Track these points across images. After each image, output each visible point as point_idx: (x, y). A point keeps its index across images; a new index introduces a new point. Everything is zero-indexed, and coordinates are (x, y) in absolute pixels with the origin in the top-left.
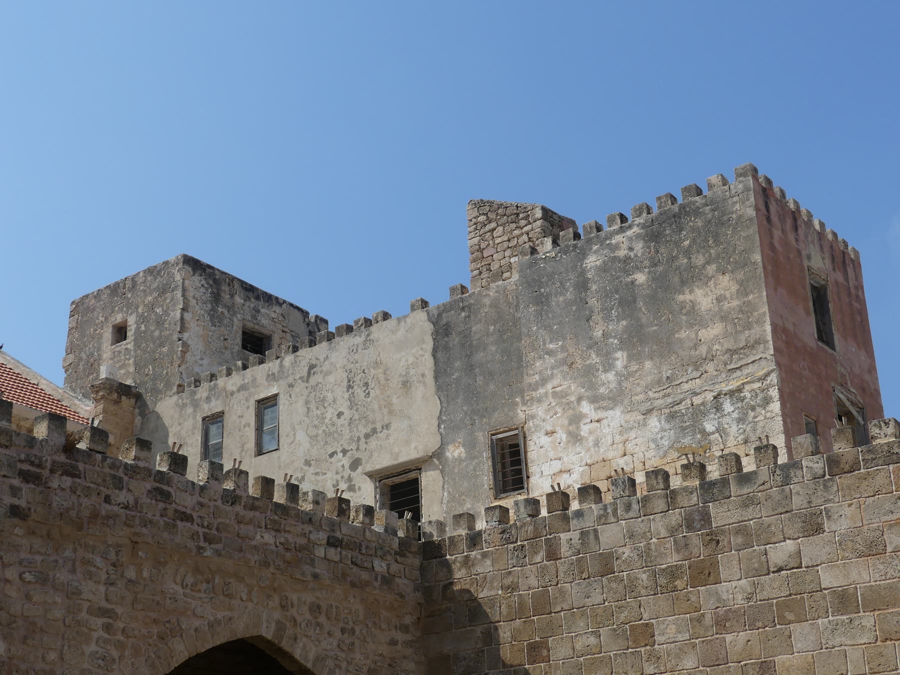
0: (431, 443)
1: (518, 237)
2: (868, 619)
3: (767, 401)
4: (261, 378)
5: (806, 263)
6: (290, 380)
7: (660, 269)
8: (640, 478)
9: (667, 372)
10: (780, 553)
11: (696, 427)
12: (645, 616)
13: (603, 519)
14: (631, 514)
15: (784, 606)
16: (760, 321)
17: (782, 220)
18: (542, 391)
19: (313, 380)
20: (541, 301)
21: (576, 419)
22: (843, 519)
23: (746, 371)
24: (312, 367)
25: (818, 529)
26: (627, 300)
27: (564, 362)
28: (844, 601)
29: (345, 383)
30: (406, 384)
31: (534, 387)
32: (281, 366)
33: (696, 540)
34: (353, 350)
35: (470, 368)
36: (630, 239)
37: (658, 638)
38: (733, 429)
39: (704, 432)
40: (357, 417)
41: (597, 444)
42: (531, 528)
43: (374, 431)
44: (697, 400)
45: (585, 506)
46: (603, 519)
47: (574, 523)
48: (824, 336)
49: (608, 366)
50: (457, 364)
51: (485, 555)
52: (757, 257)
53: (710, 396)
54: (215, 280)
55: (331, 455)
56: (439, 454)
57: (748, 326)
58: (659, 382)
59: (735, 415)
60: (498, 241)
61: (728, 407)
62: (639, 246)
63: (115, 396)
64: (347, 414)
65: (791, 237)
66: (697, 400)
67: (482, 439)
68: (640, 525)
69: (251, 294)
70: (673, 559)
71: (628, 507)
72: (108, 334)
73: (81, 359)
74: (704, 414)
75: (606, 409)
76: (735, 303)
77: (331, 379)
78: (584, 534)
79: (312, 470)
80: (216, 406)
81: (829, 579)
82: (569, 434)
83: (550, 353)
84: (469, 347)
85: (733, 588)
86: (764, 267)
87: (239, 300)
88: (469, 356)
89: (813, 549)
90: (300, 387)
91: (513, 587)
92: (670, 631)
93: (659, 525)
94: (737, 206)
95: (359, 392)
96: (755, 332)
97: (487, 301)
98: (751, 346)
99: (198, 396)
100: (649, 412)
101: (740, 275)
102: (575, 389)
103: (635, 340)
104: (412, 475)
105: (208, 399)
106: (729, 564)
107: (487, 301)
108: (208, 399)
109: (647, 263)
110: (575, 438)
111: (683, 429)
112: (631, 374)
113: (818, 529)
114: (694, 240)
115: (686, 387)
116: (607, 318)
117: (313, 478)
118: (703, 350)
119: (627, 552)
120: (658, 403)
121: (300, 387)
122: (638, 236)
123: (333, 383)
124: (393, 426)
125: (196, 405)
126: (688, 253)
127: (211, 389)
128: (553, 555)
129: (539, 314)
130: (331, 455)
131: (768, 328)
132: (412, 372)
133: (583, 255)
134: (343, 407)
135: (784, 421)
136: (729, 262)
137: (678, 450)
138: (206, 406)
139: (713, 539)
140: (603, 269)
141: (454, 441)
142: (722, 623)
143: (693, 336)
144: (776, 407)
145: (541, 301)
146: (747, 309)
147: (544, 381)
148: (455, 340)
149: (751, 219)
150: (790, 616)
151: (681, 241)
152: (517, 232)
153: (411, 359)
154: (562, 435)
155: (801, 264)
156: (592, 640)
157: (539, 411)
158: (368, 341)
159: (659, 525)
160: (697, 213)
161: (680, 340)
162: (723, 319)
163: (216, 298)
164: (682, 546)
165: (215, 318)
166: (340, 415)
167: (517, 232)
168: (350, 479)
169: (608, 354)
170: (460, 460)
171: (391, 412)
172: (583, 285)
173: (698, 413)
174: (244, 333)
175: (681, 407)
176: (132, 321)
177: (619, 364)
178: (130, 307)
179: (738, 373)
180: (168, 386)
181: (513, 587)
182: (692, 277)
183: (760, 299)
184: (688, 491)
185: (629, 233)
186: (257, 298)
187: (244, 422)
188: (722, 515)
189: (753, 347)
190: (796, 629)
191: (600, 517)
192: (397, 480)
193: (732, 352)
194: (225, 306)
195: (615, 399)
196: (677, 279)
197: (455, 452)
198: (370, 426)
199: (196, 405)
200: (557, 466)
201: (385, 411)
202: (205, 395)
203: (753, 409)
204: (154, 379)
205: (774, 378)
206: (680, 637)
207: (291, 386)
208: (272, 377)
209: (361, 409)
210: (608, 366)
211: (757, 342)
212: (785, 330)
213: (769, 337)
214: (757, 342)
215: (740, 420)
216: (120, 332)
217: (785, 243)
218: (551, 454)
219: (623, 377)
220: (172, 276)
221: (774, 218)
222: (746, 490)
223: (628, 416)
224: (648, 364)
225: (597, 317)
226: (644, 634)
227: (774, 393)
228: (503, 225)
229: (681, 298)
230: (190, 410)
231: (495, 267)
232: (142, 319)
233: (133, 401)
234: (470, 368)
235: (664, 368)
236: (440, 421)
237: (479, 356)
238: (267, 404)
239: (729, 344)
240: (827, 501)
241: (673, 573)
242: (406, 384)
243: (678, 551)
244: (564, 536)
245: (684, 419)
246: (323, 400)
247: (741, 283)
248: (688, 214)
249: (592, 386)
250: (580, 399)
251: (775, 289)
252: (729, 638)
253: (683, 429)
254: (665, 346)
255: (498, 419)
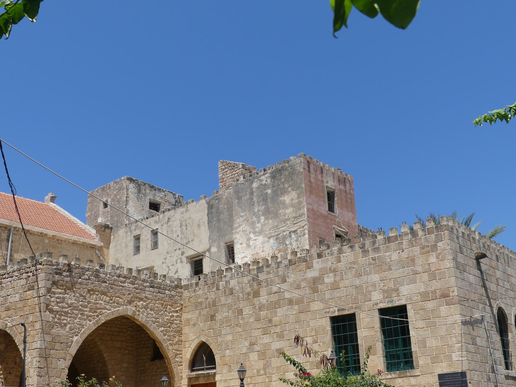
0: (207, 247)
1: (234, 174)
2: (296, 307)
3: (304, 234)
4: (153, 223)
5: (325, 185)
6: (162, 223)
7: (275, 188)
8: (269, 259)
9: (276, 224)
10: (275, 289)
11: (284, 243)
12: (241, 307)
13: (231, 278)
14: (239, 276)
15: (276, 303)
16: (303, 208)
17: (316, 171)
18: (239, 229)
19: (170, 223)
20: (239, 198)
21: (249, 239)
22: (292, 278)
23: (299, 224)
24: (169, 219)
25: (285, 281)
26: (264, 199)
27: (245, 220)
28: (290, 302)
29: (180, 225)
30: (199, 225)
31: (237, 228)
32: (159, 218)
33: (255, 284)
34: (182, 213)
35: (219, 220)
36: (266, 178)
37: (244, 313)
38: (294, 244)
39: (286, 245)
40: (183, 237)
41: (255, 248)
42: (212, 280)
43: (189, 242)
44: (285, 233)
45: (227, 274)
46: (231, 278)
47: (223, 279)
48: (331, 208)
49: (259, 222)
50: (215, 219)
51: (200, 289)
52: (303, 186)
53: (288, 232)
54: (138, 185)
55: (175, 250)
56: (209, 250)
57: (300, 209)
58: (273, 227)
59: (295, 239)
60: (228, 175)
61: (293, 236)
62: (269, 180)
63: (103, 229)
64: (180, 236)
65: (319, 177)
66: (285, 233)
67: (223, 245)
68: (240, 280)
69: (152, 189)
70: (249, 290)
71: (238, 274)
72: (102, 205)
73: (92, 214)
74: (286, 238)
75: (258, 236)
76: (297, 201)
77: (175, 223)
78: (226, 282)
79: (169, 255)
80: (138, 232)
81: (287, 295)
82: (247, 244)
83: (242, 216)
84: (219, 213)
85: (264, 298)
86: (306, 189)
87: (148, 191)
88: (219, 216)
89: (284, 286)
90: (165, 226)
91: (207, 298)
92: (247, 311)
93: (246, 280)
94: (298, 168)
95: (184, 228)
96: (301, 211)
97: (224, 197)
98: (300, 216)
99: (132, 229)
100: (271, 237)
101: (298, 192)
102: (248, 229)
103: (267, 213)
104: (201, 257)
105: (135, 230)
106: (263, 292)
107: (224, 197)
108: (135, 230)
109: (271, 186)
110: (248, 246)
111: (280, 243)
112: (265, 224)
113: (285, 281)
114: (285, 179)
115: (281, 229)
116: (259, 205)
117: (169, 258)
118: (287, 216)
119: (237, 288)
120: (273, 234)
121: (165, 226)
122: (269, 177)
123: (175, 224)
124: (195, 241)
125: (131, 231)
126: (283, 183)
127: (136, 226)
128: (218, 289)
129: (239, 203)
130: (175, 250)
131: (306, 210)
132: (201, 221)
133: (252, 183)
134: (179, 233)
135: (309, 241)
136: (296, 187)
137: (278, 250)
138: (134, 232)
139: (259, 284)
140: (258, 188)
141: (213, 246)
142: (260, 309)
143: (284, 212)
144: (307, 236)
145: (239, 198)
146: (300, 203)
147: (239, 226)
148: (214, 210)
149: (302, 173)
150: (277, 306)
151: (282, 179)
152: (234, 172)
153: (200, 217)
154: (244, 245)
155: (323, 186)
156: (227, 314)
157: (237, 236)
158: (187, 211)
159: (246, 280)
160: (286, 169)
161: (280, 213)
162: (293, 206)
163: (139, 191)
164: (251, 286)
165: (139, 199)
166: (178, 236)
167: (234, 172)
168: (181, 259)
169: (259, 217)
170: (215, 252)
171: (194, 235)
172: (252, 193)
173: (284, 238)
174: (150, 203)
175: (280, 236)
176: (109, 200)
177: (262, 221)
178: (108, 195)
179: (296, 225)
180: (122, 224)
181: (207, 298)
182: (284, 192)
183: (303, 199)
184: (254, 269)
185: (266, 176)
186: (155, 190)
187: (147, 238)
188: (262, 277)
189: (301, 216)
190: (279, 310)
191: (230, 277)
192: (197, 259)
193: (295, 218)
194: (143, 194)
195: (261, 233)
196: (280, 192)
197: (214, 249)
198: (188, 240)
199: (131, 231)
200: (243, 255)
201: (192, 235)
202: (134, 228)
203: (300, 237)
204: (117, 222)
205: (306, 227)
206: (250, 313)
207: (162, 225)
208: (156, 222)
209: (185, 234)
210: (259, 222)
211: (302, 215)
212: (313, 210)
213: (306, 213)
214: (302, 215)
215: (297, 241)
216: (106, 205)
217: (316, 179)
218: (241, 251)
219: (263, 225)
220: (122, 184)
221: (312, 170)
222: (268, 270)
223: (264, 239)
224: (270, 221)
225: (256, 204)
226: (240, 312)
227: (306, 231)
228: (230, 170)
229: (281, 199)
230: (129, 233)
231: (227, 185)
232: (113, 200)
233: (110, 230)
234: (219, 220)
235: (275, 223)
236: (210, 239)
237: (222, 216)
238: (155, 233)
239: (294, 215)
240: (288, 273)
241: (248, 294)
242: (199, 225)
243: (250, 287)
244: (221, 283)
245: (281, 240)
246: (173, 231)
247: (298, 195)
248: (283, 170)
249: (254, 228)
250: (250, 233)
251: (310, 196)
252: (262, 313)
253: (280, 243)
254: (276, 215)
255: (227, 239)
